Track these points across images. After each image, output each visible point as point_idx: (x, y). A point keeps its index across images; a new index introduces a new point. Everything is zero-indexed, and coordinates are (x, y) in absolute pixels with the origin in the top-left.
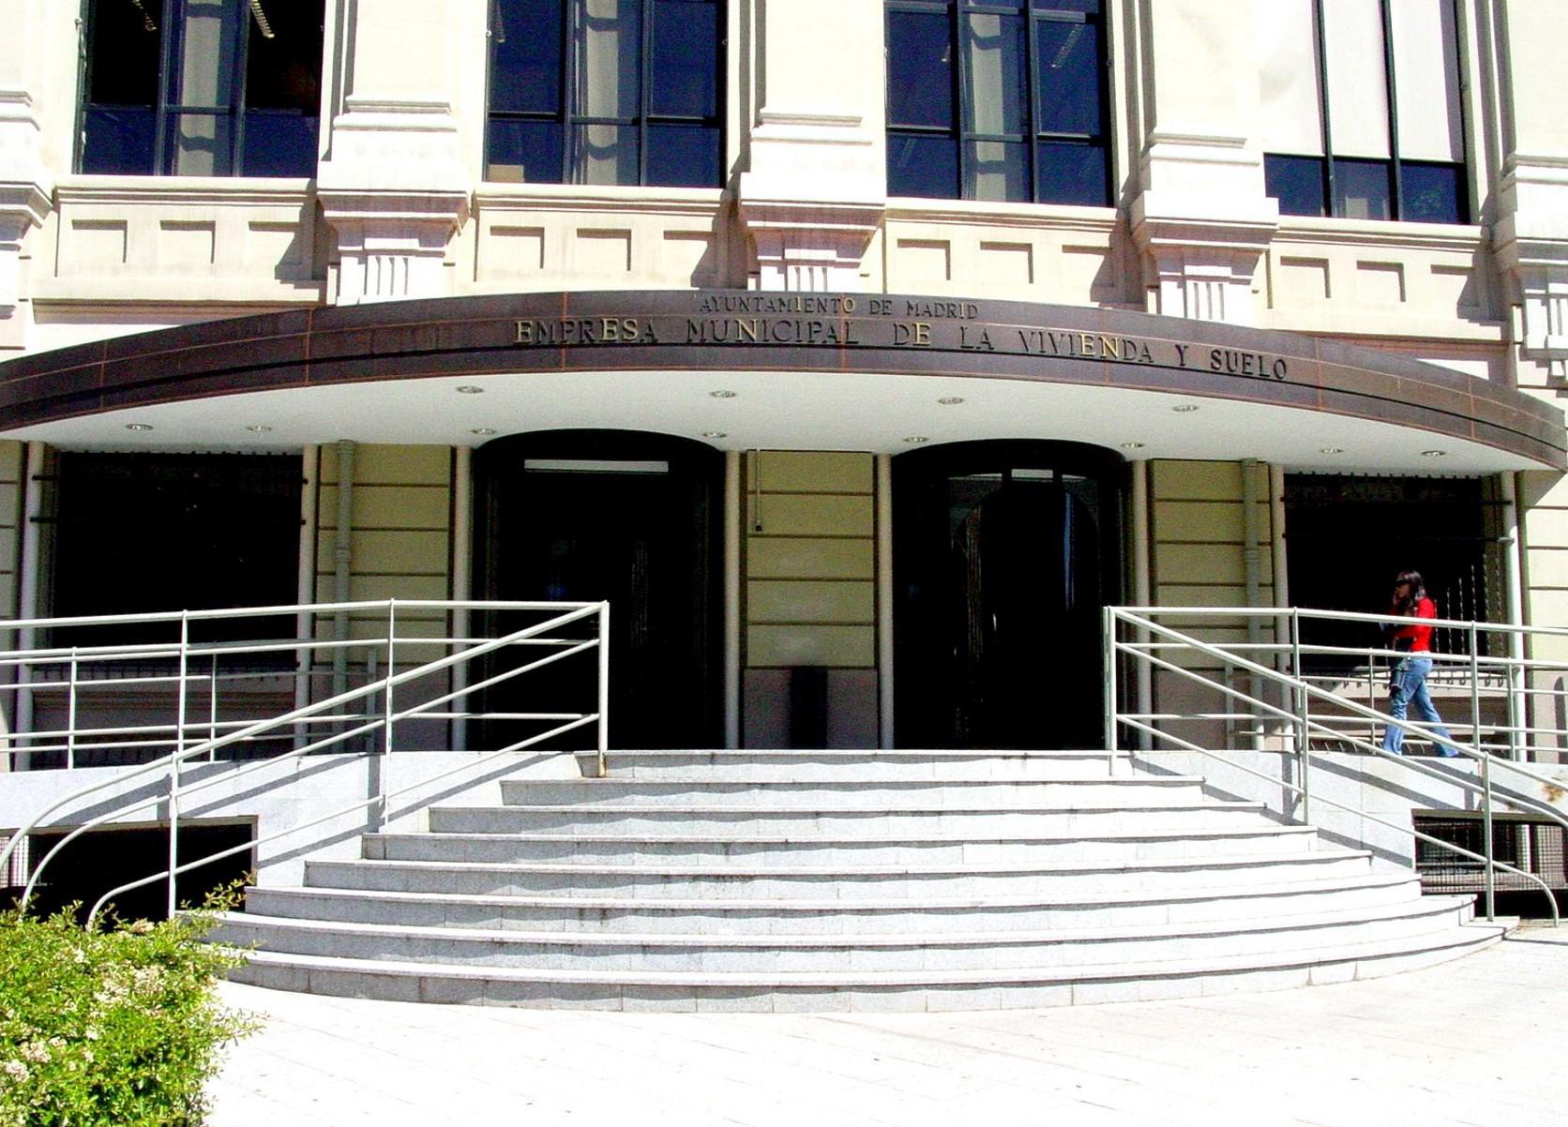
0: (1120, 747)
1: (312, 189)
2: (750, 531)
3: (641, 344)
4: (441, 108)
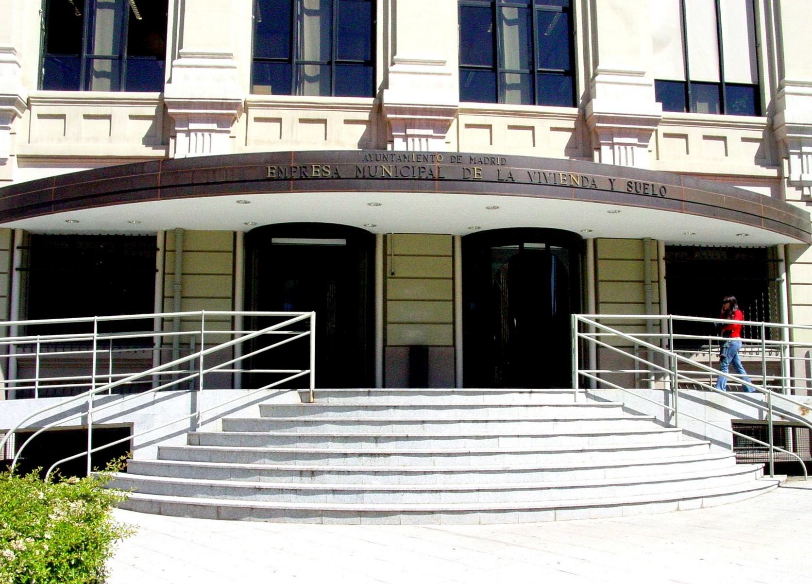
0: (580, 387)
1: (162, 98)
2: (388, 275)
3: (332, 178)
4: (228, 56)
